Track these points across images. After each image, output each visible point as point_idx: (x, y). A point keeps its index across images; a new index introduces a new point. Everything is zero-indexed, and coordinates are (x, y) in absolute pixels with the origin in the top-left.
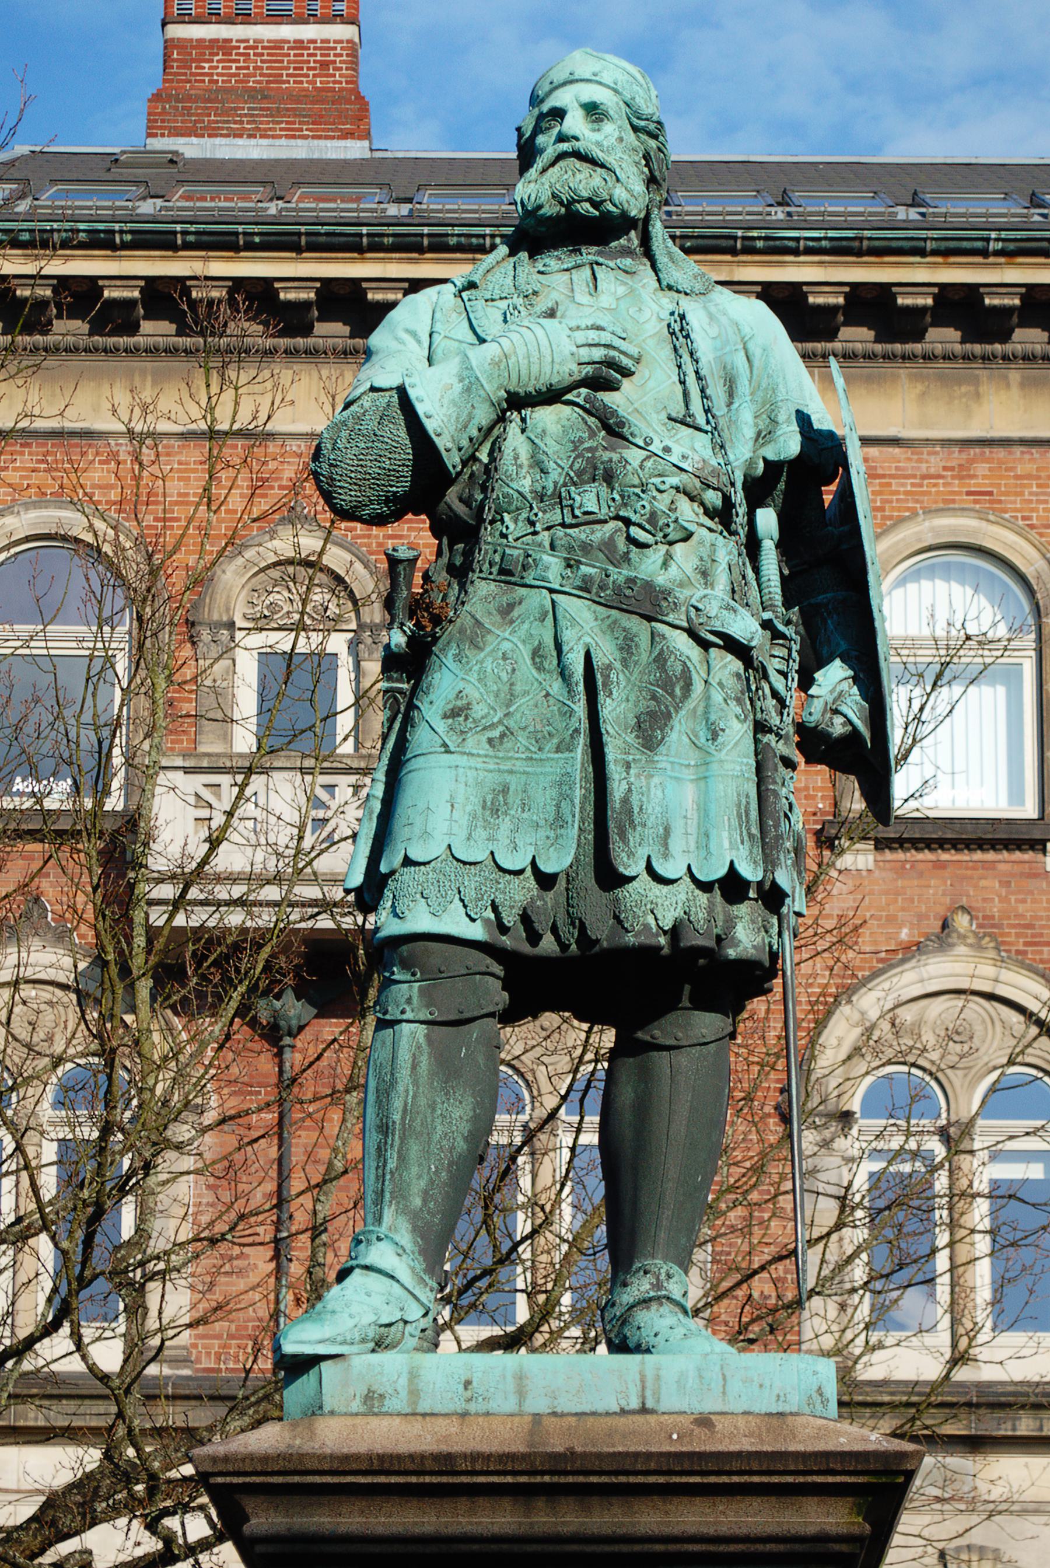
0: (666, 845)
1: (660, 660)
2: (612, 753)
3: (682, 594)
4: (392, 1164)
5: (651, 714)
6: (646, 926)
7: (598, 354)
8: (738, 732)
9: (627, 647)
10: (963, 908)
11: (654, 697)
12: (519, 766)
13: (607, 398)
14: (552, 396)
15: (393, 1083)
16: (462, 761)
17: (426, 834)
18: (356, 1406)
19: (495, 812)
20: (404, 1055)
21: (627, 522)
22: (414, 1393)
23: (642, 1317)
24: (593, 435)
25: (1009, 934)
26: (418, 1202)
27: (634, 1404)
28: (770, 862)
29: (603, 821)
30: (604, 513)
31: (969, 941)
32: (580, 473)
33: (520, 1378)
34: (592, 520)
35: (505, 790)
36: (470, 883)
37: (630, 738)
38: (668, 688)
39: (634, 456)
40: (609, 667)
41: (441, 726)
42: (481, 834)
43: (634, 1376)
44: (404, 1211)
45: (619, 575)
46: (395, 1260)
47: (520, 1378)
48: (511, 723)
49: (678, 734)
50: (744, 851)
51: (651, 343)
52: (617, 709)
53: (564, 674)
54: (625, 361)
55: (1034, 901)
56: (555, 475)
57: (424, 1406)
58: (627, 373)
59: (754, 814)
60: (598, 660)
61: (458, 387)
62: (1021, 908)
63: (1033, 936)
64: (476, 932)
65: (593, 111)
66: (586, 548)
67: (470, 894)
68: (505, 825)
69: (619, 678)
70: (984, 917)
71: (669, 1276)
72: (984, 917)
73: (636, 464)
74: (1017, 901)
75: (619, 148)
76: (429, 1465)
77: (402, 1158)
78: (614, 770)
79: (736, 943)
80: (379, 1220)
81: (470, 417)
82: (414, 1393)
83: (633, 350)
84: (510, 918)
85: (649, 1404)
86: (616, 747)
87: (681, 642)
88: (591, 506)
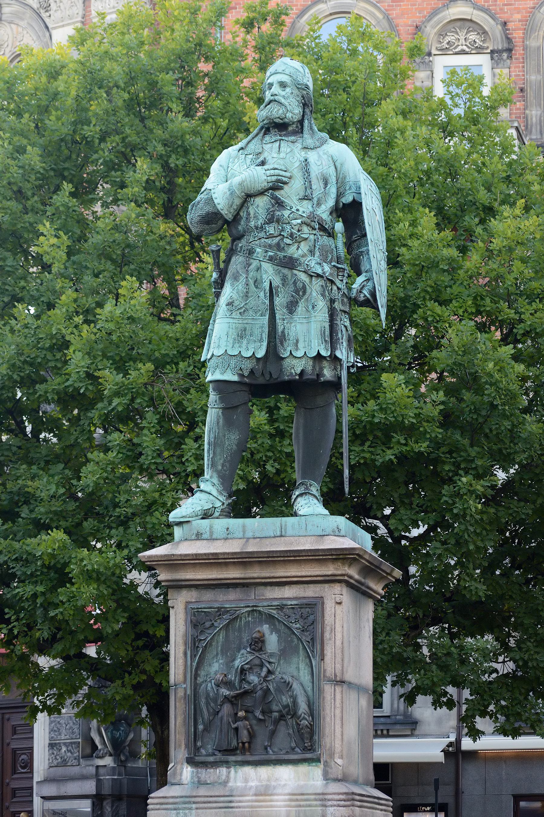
0: (297, 346)
2: (278, 316)
3: (302, 260)
5: (291, 302)
6: (291, 373)
7: (274, 178)
8: (322, 305)
9: (284, 279)
11: (292, 296)
12: (250, 321)
13: (277, 193)
14: (261, 193)
18: (194, 537)
19: (242, 337)
22: (211, 533)
24: (273, 206)
27: (279, 534)
29: (275, 338)
32: (269, 220)
33: (244, 526)
35: (245, 330)
36: (233, 362)
37: (285, 310)
38: (301, 291)
40: (278, 287)
42: (237, 345)
43: (278, 525)
45: (281, 254)
46: (212, 488)
47: (244, 526)
48: (247, 307)
49: (301, 308)
50: (323, 346)
51: (296, 170)
57: (214, 536)
58: (285, 183)
59: (327, 333)
61: (228, 193)
64: (235, 378)
65: (283, 85)
66: (270, 246)
68: (245, 342)
69: (281, 290)
71: (311, 485)
73: (286, 216)
75: (291, 96)
76: (211, 557)
79: (324, 375)
81: (233, 203)
82: (211, 533)
85: (283, 534)
87: (303, 277)
88: (272, 232)
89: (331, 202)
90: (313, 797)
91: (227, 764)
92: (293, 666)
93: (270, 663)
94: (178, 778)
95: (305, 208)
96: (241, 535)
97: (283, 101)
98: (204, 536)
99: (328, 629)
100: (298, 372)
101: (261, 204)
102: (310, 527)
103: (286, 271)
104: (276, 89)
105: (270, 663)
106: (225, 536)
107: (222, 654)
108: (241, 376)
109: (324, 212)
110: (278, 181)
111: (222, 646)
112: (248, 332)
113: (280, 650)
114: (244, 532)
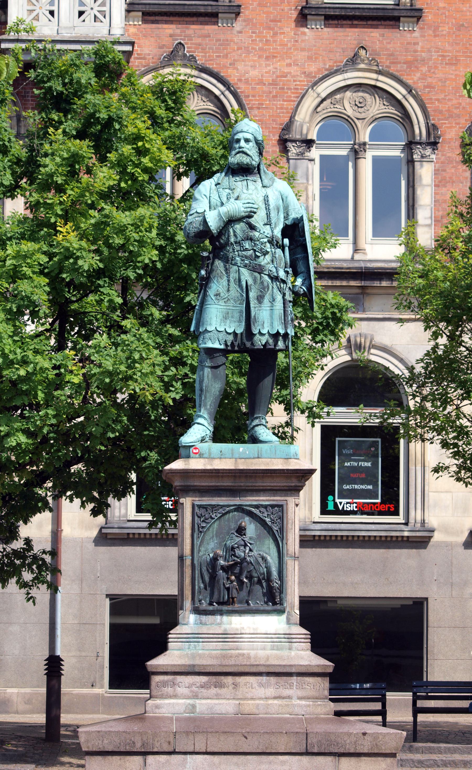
1: (262, 283)
2: (252, 305)
4: (203, 398)
5: (260, 296)
8: (279, 297)
9: (255, 280)
10: (362, 47)
15: (203, 380)
16: (219, 307)
17: (211, 324)
20: (206, 374)
21: (255, 251)
22: (210, 454)
23: (257, 428)
25: (382, 58)
26: (208, 407)
27: (256, 456)
28: (286, 328)
30: (250, 248)
31: (366, 62)
34: (246, 250)
36: (221, 336)
38: (263, 289)
39: (257, 234)
41: (213, 298)
42: (223, 324)
43: (256, 450)
44: (206, 409)
47: (232, 450)
50: (280, 327)
52: (252, 295)
53: (242, 289)
54: (255, 210)
55: (394, 43)
56: (239, 239)
57: (212, 456)
58: (255, 213)
60: (249, 283)
62: (389, 46)
63: (394, 59)
64: (222, 347)
65: (247, 141)
66: (246, 257)
67: (220, 338)
70: (372, 50)
72: (372, 50)
74: (387, 43)
77: (205, 397)
78: (252, 309)
80: (200, 411)
83: (256, 207)
84: (229, 344)
86: (253, 303)
87: (266, 278)
89: (281, 226)
90: (283, 636)
91: (221, 613)
92: (266, 546)
93: (251, 544)
94: (187, 620)
95: (267, 230)
96: (231, 456)
97: (249, 152)
98: (205, 456)
99: (290, 521)
100: (264, 343)
101: (239, 228)
102: (278, 452)
103: (257, 274)
104: (242, 143)
105: (251, 544)
106: (219, 456)
107: (217, 537)
108: (226, 345)
109: (278, 233)
110: (251, 212)
111: (217, 531)
112: (230, 315)
113: (256, 535)
114: (232, 454)
